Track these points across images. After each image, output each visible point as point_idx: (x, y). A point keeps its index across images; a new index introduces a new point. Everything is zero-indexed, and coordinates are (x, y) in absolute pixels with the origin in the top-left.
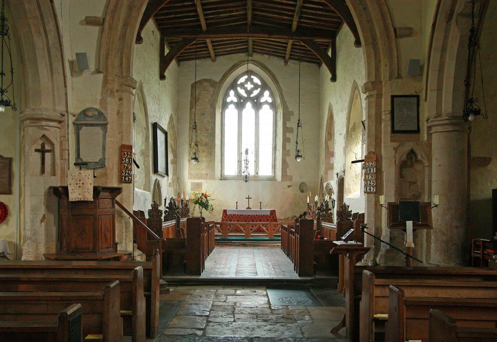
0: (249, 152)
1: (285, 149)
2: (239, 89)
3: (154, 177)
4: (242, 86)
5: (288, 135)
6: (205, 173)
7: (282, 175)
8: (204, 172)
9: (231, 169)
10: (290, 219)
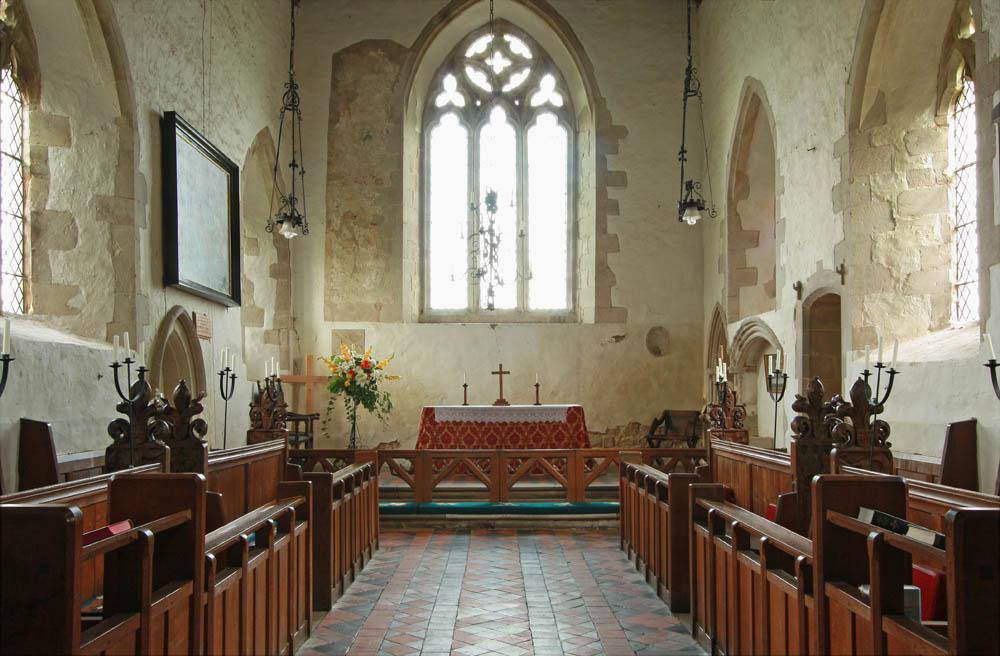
0: (499, 203)
1: (605, 232)
2: (469, 71)
3: (161, 302)
4: (479, 62)
5: (612, 193)
6: (374, 302)
7: (599, 308)
8: (370, 300)
9: (448, 293)
10: (622, 431)
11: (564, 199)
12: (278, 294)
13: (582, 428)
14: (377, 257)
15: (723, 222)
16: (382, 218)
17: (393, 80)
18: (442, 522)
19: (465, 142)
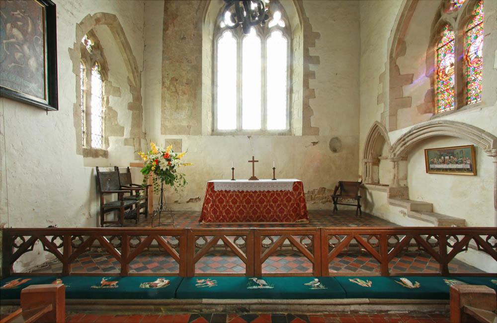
9: (226, 122)
11: (268, 117)
12: (134, 118)
13: (302, 195)
14: (188, 101)
15: (384, 73)
16: (192, 81)
17: (197, 8)
18: (199, 306)
19: (235, 45)
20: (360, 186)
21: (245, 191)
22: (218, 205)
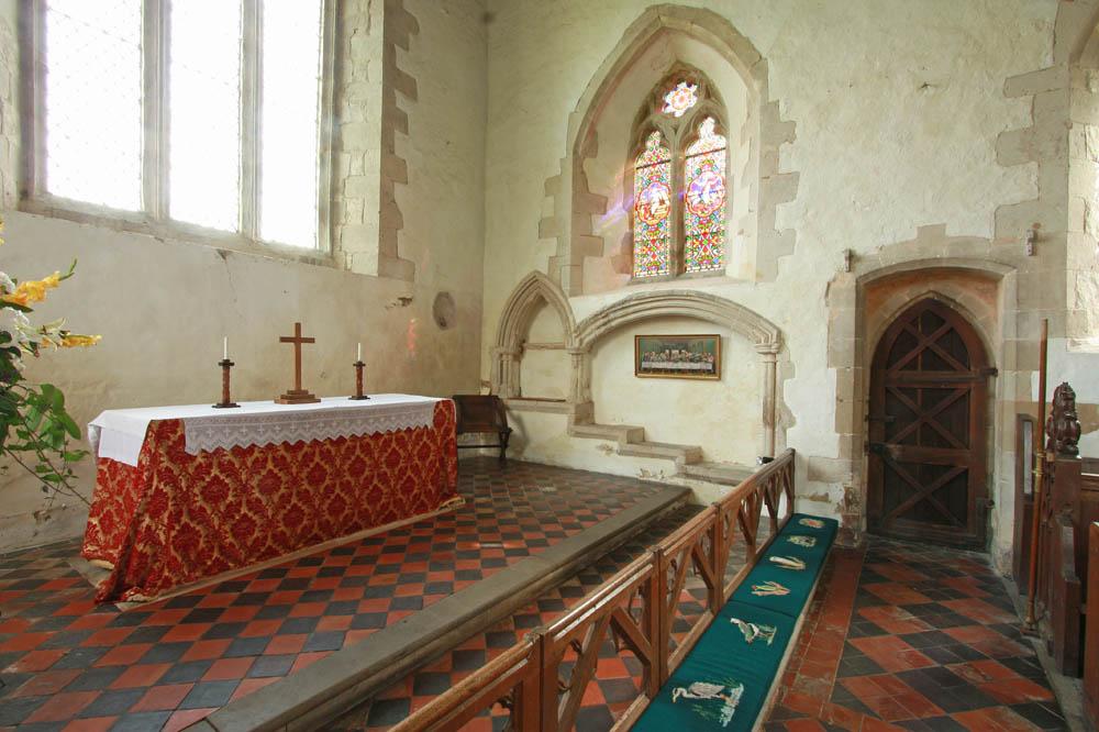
20: (492, 401)
21: (347, 438)
22: (202, 509)
